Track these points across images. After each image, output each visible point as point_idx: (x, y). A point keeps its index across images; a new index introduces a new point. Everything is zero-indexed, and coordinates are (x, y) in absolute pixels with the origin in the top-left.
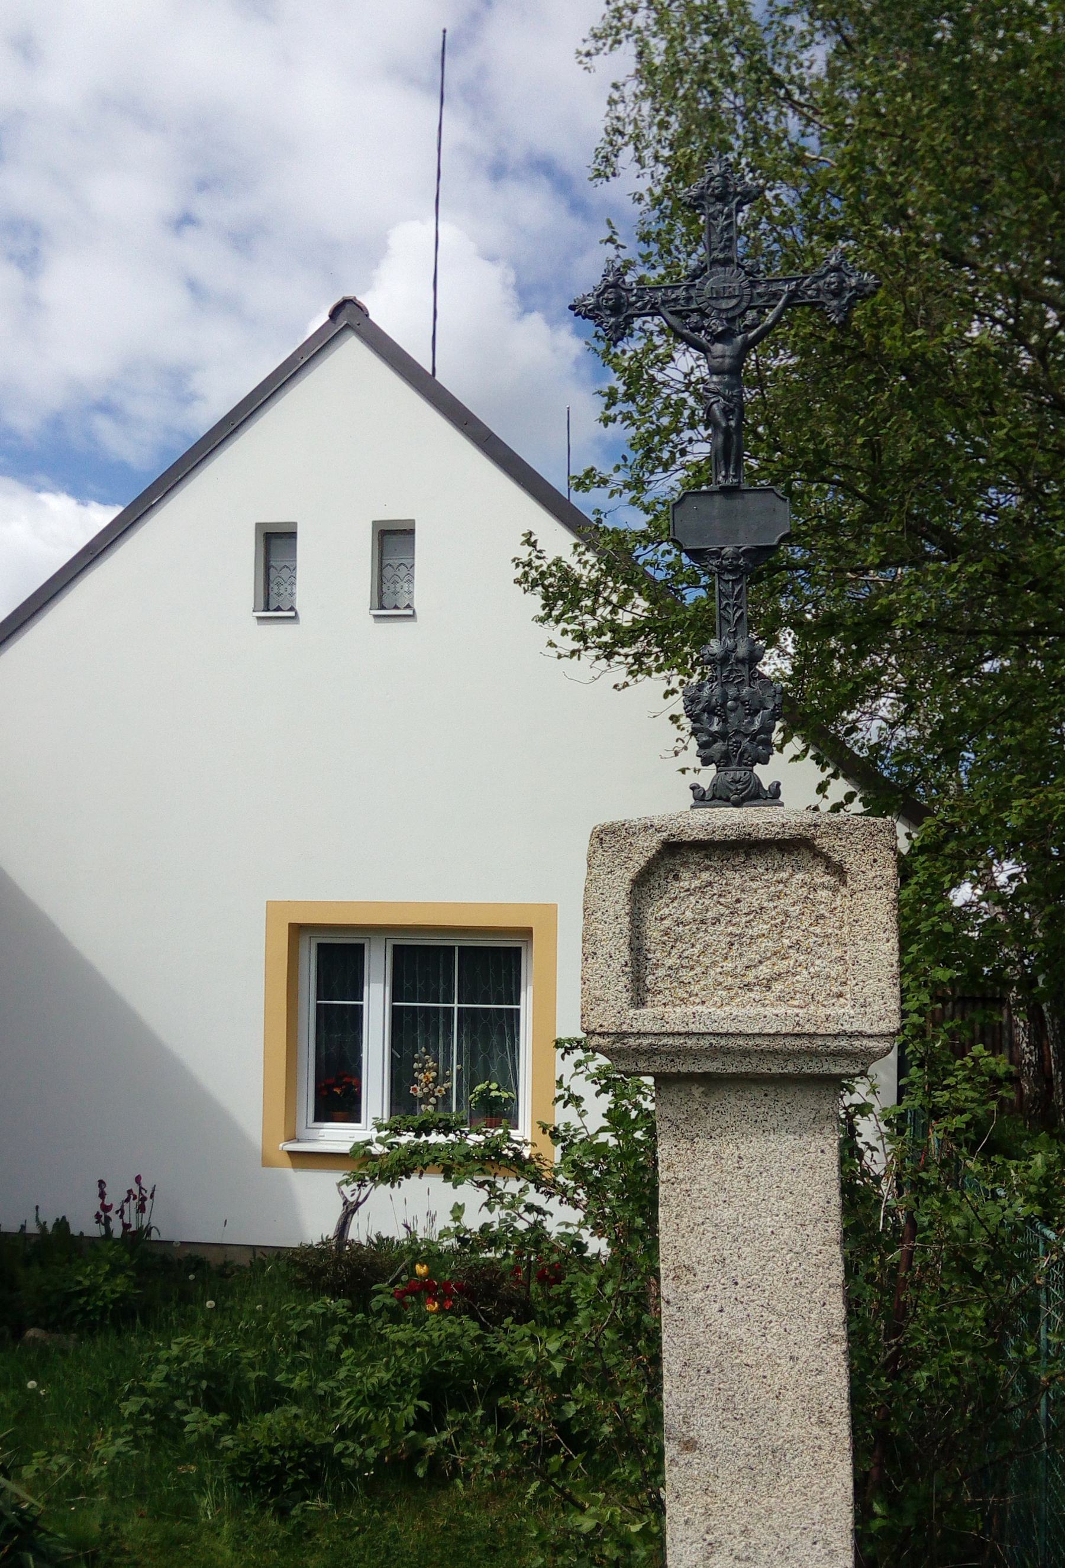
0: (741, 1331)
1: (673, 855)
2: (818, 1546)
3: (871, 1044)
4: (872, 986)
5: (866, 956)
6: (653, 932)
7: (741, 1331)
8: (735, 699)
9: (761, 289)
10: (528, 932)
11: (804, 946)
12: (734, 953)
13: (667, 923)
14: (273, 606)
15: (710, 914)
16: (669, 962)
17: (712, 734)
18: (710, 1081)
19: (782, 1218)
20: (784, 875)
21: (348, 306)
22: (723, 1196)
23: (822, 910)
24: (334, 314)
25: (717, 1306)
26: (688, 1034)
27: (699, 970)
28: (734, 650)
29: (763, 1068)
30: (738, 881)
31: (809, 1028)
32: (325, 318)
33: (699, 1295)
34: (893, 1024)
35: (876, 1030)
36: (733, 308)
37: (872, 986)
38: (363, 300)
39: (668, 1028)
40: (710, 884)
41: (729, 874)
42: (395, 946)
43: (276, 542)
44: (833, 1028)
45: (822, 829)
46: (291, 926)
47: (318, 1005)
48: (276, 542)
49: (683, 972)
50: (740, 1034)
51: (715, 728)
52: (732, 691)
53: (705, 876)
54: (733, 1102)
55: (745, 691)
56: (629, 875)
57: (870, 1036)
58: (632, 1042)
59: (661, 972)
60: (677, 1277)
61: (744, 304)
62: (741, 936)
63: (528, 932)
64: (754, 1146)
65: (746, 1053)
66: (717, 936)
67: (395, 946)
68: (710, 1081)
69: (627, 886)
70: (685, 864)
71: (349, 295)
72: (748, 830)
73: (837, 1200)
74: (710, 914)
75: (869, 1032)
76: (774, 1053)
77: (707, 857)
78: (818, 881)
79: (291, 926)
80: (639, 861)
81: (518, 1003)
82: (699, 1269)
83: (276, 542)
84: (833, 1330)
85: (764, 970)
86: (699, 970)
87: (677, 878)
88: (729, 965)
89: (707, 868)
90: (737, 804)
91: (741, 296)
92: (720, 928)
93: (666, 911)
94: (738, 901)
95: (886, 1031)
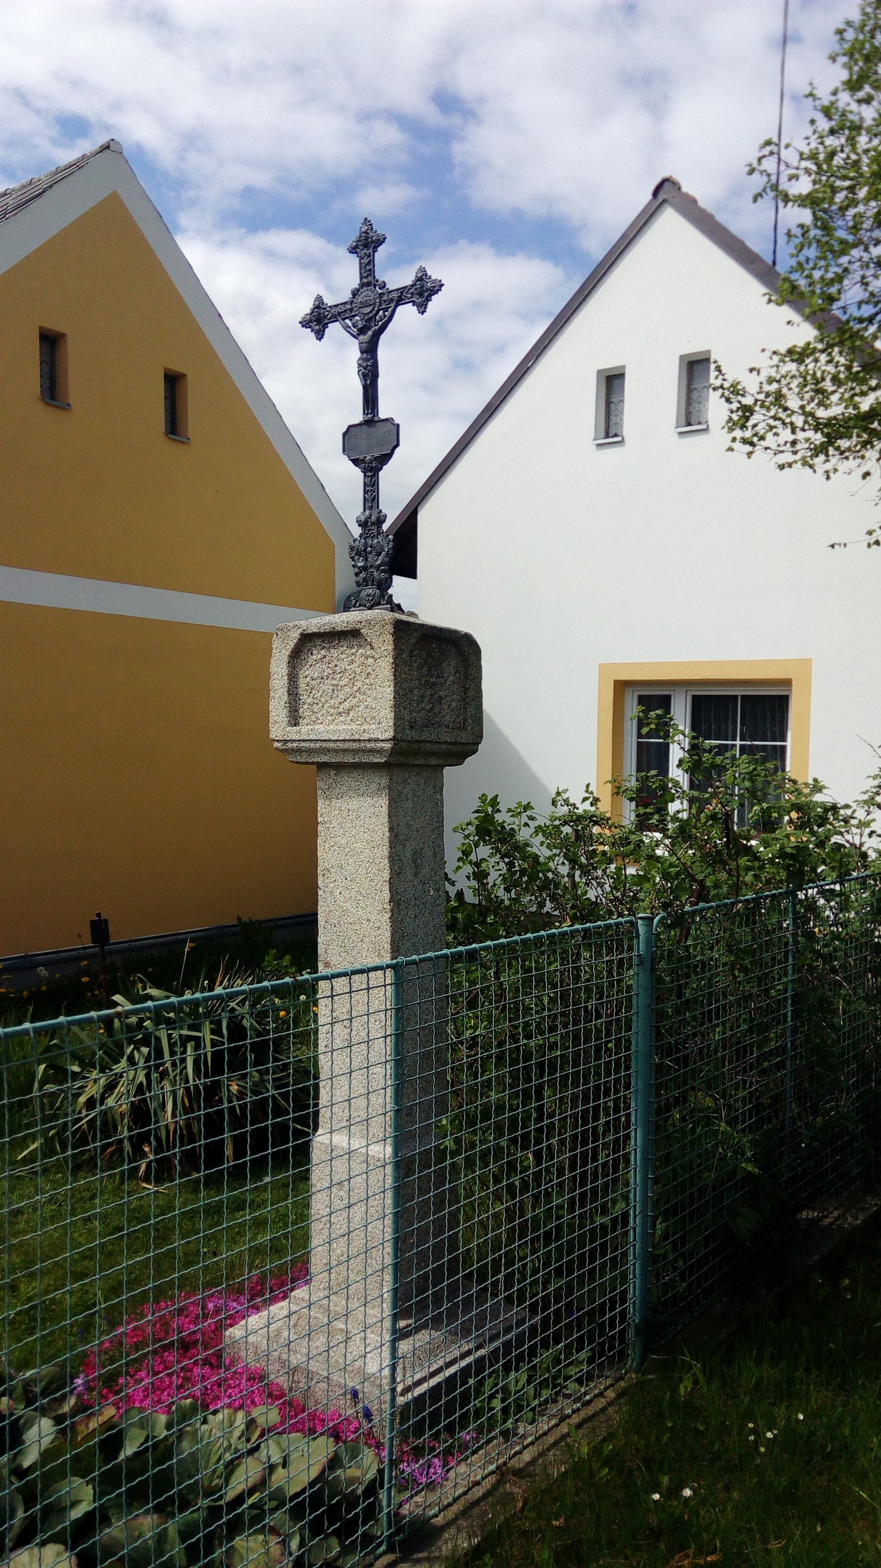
0: (348, 905)
1: (310, 641)
2: (377, 1023)
3: (384, 745)
4: (382, 714)
5: (380, 696)
6: (302, 683)
7: (348, 905)
8: (371, 547)
9: (385, 298)
10: (788, 683)
11: (362, 690)
12: (334, 696)
13: (308, 679)
14: (612, 433)
15: (325, 674)
16: (309, 701)
17: (359, 568)
18: (339, 767)
19: (365, 843)
20: (354, 650)
21: (666, 184)
22: (342, 831)
23: (370, 670)
24: (656, 193)
25: (338, 891)
26: (311, 741)
27: (320, 705)
28: (370, 518)
29: (366, 759)
30: (335, 655)
31: (357, 737)
32: (649, 197)
33: (332, 885)
34: (390, 734)
35: (383, 738)
36: (370, 312)
37: (382, 714)
38: (677, 177)
39: (302, 738)
40: (325, 657)
41: (332, 651)
42: (694, 697)
43: (612, 382)
44: (366, 736)
45: (363, 624)
46: (617, 683)
47: (639, 743)
48: (612, 382)
49: (314, 706)
50: (330, 740)
51: (360, 564)
52: (369, 541)
53: (323, 652)
54: (347, 780)
55: (375, 541)
56: (288, 653)
57: (383, 741)
58: (290, 745)
59: (306, 707)
60: (323, 875)
61: (376, 309)
62: (337, 685)
63: (788, 683)
64: (354, 803)
65: (336, 751)
66: (327, 686)
67: (694, 697)
68: (339, 767)
69: (286, 659)
70: (315, 646)
71: (666, 175)
72: (334, 626)
73: (387, 834)
74: (325, 674)
75: (381, 738)
76: (345, 751)
77: (323, 641)
78: (368, 653)
79: (617, 683)
80: (291, 645)
81: (784, 740)
82: (332, 870)
83: (697, 367)
84: (385, 906)
85: (346, 705)
86: (320, 705)
87: (312, 654)
88: (332, 702)
89: (323, 648)
90: (370, 608)
91: (374, 304)
92: (329, 681)
93: (307, 673)
94: (336, 666)
95: (388, 738)
